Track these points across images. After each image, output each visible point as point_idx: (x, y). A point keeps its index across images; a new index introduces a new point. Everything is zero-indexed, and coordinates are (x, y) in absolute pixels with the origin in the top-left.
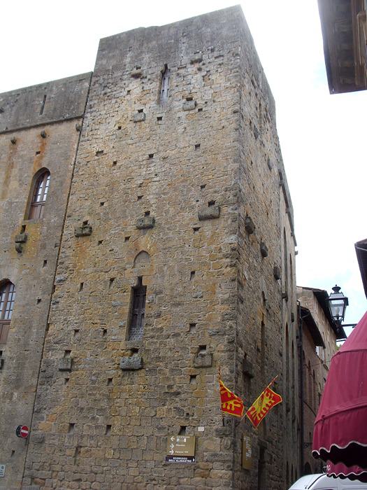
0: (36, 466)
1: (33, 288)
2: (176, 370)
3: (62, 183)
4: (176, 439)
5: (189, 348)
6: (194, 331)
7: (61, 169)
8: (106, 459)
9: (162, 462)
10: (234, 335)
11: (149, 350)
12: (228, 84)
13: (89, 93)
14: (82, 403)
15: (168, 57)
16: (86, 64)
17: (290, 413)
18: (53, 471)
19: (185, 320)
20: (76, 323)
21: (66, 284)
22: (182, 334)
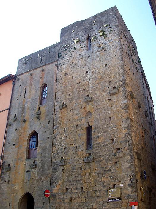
3: (52, 88)
9: (106, 201)
14: (70, 179)
16: (57, 39)
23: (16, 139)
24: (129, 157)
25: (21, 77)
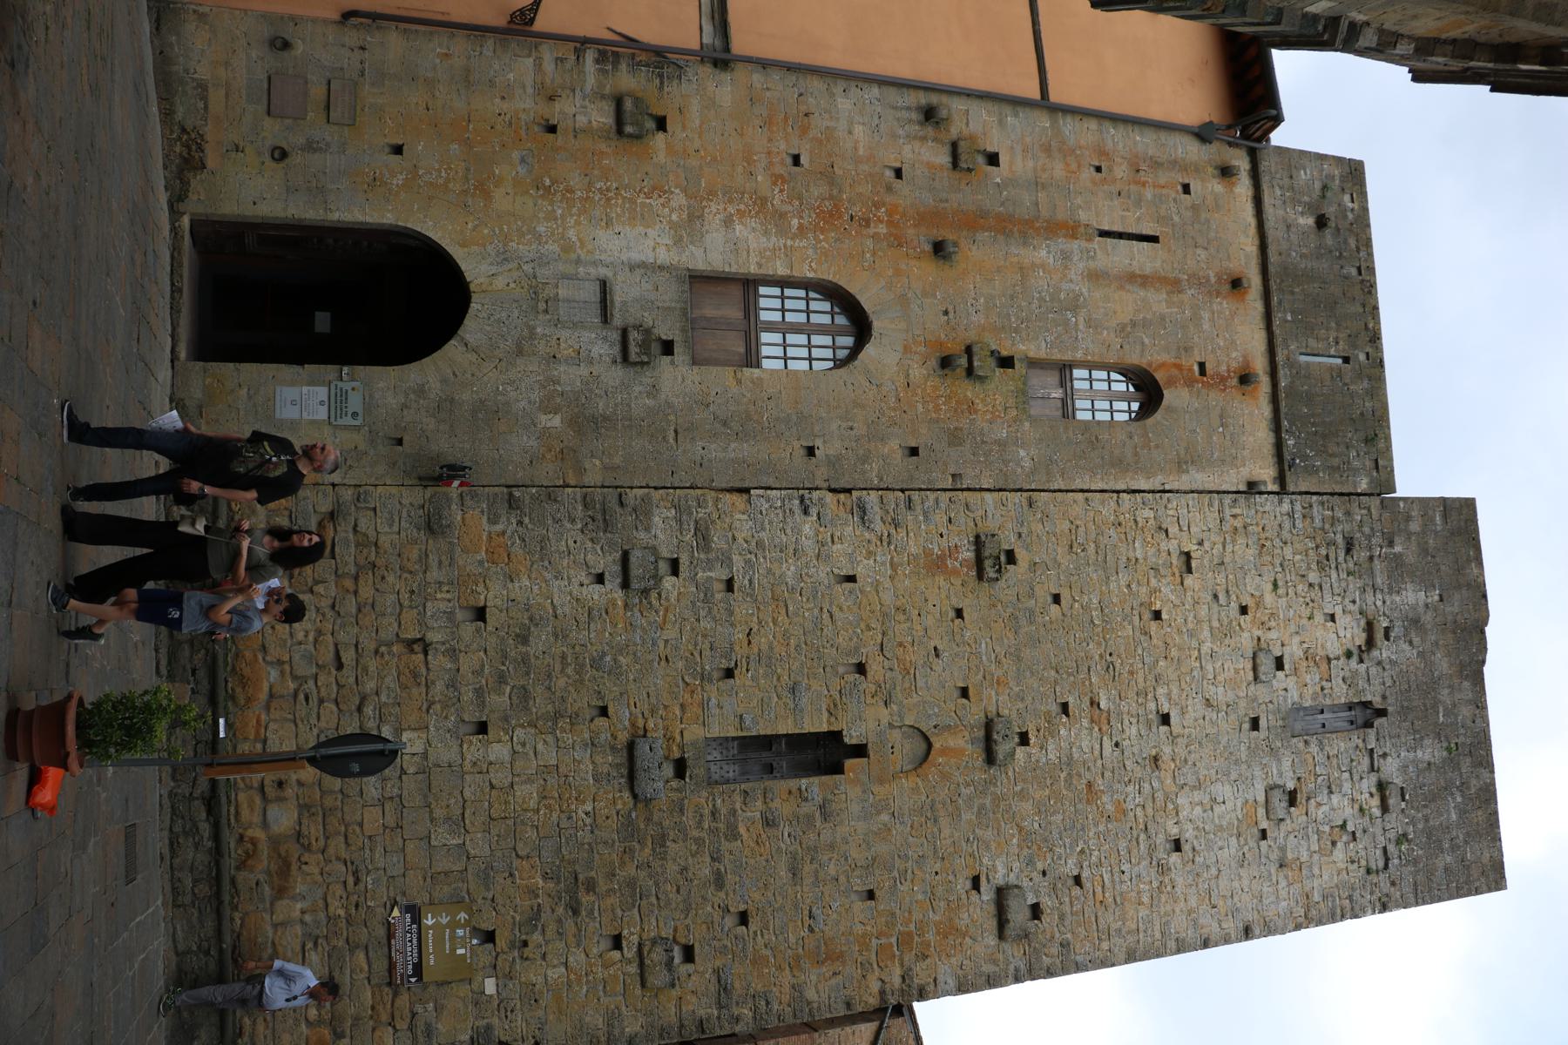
1: (844, 425)
2: (633, 896)
4: (463, 927)
5: (688, 921)
9: (404, 894)
11: (682, 810)
12: (1317, 897)
14: (540, 641)
18: (356, 578)
19: (757, 896)
22: (722, 895)
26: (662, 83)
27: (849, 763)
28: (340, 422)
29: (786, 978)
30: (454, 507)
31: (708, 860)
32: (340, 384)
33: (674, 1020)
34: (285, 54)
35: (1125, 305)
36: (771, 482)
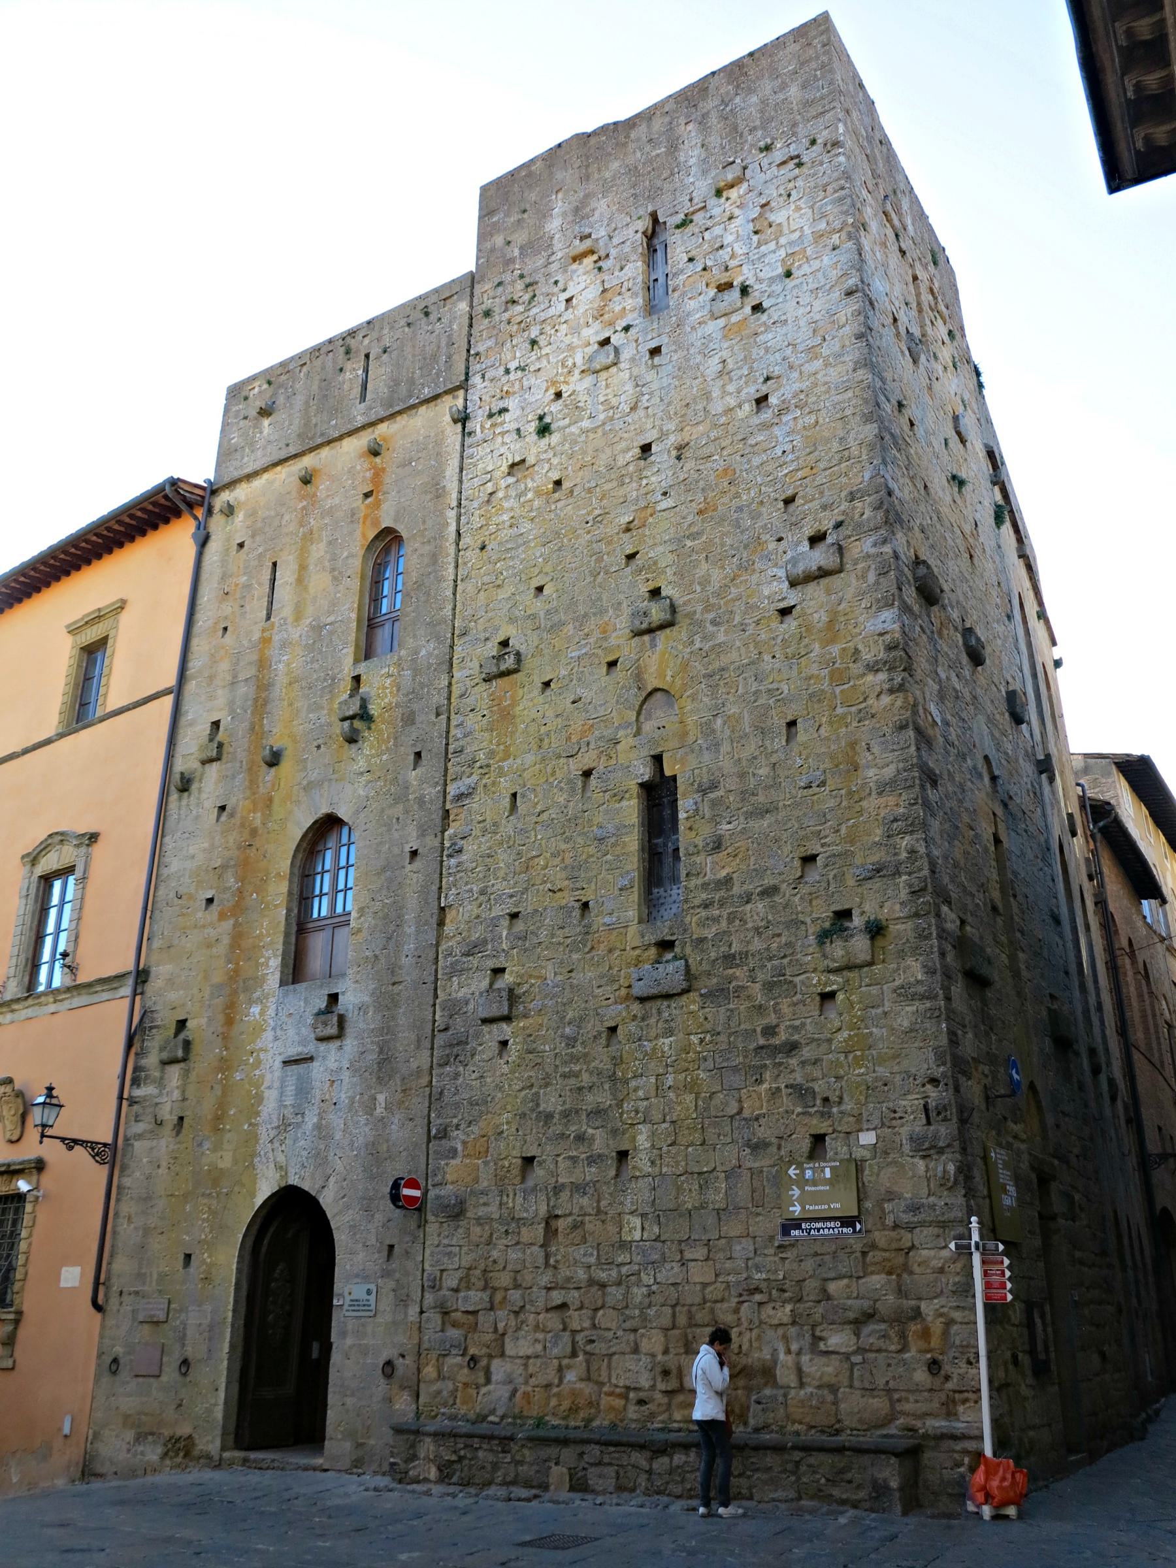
0: (451, 1281)
3: (434, 558)
6: (813, 875)
7: (429, 523)
8: (624, 1245)
9: (772, 1238)
10: (926, 872)
12: (822, 225)
13: (471, 326)
14: (551, 1102)
15: (654, 193)
16: (458, 256)
17: (1103, 1078)
18: (495, 1289)
19: (787, 849)
20: (511, 896)
21: (474, 804)
23: (220, 871)
24: (910, 961)
25: (243, 498)
26: (155, 1027)
27: (668, 772)
28: (373, 1307)
29: (871, 803)
30: (442, 1193)
31: (749, 907)
32: (346, 1307)
33: (910, 925)
34: (122, 1361)
35: (319, 581)
36: (435, 888)
